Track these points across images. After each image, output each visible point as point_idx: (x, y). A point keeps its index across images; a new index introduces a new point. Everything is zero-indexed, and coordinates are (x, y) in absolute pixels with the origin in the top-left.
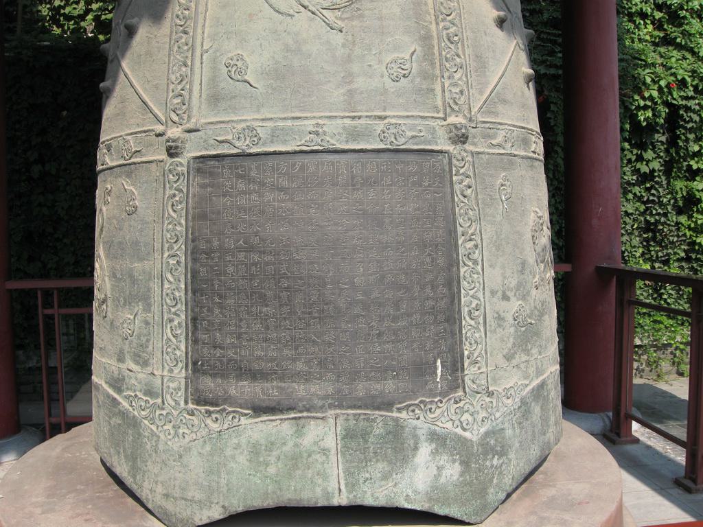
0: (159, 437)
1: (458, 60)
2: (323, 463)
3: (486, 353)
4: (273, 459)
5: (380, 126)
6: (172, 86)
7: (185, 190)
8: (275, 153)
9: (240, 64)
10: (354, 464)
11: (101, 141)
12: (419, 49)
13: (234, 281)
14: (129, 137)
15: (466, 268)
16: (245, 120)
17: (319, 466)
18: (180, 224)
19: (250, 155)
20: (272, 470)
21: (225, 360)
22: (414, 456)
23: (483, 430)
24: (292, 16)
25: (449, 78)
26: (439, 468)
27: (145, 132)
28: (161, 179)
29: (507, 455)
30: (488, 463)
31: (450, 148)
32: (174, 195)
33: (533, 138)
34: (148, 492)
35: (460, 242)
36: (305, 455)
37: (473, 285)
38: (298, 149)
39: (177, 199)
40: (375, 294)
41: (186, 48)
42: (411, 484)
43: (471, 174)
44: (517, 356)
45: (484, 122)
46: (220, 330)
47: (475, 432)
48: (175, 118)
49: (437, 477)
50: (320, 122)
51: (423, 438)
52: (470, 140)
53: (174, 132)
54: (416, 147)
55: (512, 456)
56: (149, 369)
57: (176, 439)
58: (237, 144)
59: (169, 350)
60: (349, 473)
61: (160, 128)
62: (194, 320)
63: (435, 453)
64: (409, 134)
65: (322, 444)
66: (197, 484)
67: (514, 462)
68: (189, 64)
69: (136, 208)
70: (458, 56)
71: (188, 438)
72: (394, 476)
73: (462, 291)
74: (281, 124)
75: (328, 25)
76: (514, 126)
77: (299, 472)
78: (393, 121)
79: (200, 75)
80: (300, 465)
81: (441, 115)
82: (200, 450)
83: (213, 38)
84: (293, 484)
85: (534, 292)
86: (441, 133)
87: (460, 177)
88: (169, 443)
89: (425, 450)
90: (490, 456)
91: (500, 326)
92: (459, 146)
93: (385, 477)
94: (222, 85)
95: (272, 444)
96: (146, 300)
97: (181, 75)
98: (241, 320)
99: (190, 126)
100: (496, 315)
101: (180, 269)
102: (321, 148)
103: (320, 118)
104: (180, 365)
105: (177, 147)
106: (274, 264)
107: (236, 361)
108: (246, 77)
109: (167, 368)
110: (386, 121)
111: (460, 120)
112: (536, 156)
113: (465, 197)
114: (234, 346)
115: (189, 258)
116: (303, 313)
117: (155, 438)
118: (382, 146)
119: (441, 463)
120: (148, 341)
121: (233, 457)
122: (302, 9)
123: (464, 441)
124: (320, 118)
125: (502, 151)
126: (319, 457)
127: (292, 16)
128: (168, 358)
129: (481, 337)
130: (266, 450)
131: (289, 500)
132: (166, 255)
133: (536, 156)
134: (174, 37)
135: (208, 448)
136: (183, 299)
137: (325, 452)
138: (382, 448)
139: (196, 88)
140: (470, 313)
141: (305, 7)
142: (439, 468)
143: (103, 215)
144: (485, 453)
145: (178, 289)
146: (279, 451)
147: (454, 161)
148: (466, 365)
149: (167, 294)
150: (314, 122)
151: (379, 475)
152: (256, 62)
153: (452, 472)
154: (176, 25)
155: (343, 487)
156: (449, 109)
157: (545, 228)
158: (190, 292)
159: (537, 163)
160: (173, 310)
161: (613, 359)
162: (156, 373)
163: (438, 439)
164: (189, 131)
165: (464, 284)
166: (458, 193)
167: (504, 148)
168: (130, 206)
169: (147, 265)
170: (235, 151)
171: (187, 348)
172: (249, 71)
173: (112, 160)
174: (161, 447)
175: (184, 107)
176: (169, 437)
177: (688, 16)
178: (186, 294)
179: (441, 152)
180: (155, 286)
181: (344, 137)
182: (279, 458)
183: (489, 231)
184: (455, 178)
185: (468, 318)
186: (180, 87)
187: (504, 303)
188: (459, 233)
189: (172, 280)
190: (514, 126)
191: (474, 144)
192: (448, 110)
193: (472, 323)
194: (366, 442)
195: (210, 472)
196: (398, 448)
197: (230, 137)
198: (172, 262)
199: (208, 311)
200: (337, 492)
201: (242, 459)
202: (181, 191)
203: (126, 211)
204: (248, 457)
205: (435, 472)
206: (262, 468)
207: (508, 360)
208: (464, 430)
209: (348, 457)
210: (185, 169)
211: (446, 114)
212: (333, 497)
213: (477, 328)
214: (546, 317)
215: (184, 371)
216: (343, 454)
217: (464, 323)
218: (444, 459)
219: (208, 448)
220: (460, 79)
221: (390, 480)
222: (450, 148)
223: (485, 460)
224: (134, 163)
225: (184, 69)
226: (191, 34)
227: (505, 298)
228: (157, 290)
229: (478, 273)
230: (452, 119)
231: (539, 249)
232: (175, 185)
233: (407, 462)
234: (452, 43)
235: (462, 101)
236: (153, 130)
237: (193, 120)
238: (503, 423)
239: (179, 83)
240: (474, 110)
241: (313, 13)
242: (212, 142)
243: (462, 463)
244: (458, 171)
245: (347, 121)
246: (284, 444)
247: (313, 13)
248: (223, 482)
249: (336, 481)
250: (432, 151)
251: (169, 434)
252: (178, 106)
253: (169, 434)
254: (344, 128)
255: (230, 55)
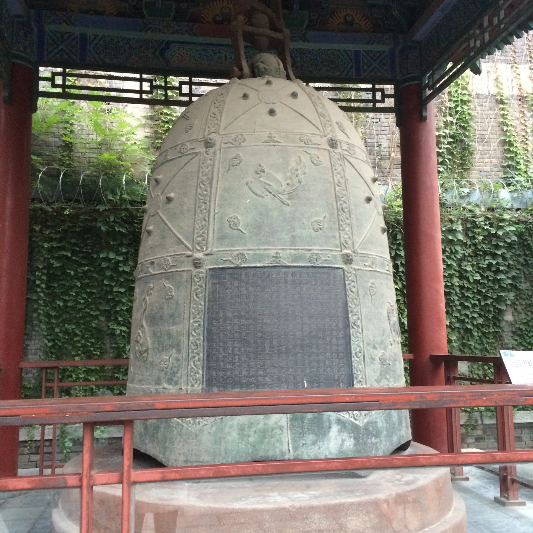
0: (183, 426)
1: (347, 221)
2: (280, 434)
3: (366, 377)
4: (252, 433)
5: (308, 254)
6: (196, 231)
7: (204, 286)
8: (255, 267)
9: (236, 221)
10: (297, 435)
11: (139, 263)
12: (327, 215)
13: (231, 334)
14: (168, 258)
15: (353, 330)
16: (238, 250)
17: (278, 436)
18: (201, 304)
19: (242, 268)
20: (251, 439)
21: (225, 377)
22: (329, 432)
23: (365, 421)
24: (263, 197)
25: (343, 230)
26: (343, 441)
27: (179, 255)
28: (190, 280)
29: (380, 438)
30: (369, 441)
31: (344, 266)
32: (198, 289)
33: (387, 263)
34: (174, 461)
35: (350, 316)
36: (270, 430)
37: (357, 339)
38: (267, 265)
39: (199, 290)
40: (307, 342)
41: (205, 211)
42: (328, 448)
43: (355, 280)
44: (382, 381)
45: (361, 253)
46: (223, 361)
47: (361, 422)
48: (199, 248)
49: (342, 445)
50: (279, 251)
51: (333, 422)
52: (353, 262)
53: (199, 255)
54: (327, 265)
55: (383, 438)
56: (178, 387)
57: (194, 426)
58: (235, 262)
59: (192, 374)
60: (294, 441)
61: (189, 253)
62: (208, 356)
63: (340, 431)
64: (323, 258)
65: (279, 424)
66: (206, 451)
67: (384, 442)
68: (207, 220)
69: (172, 296)
70: (347, 219)
71: (201, 424)
72: (319, 443)
73: (352, 342)
74: (258, 252)
75: (282, 202)
76: (377, 256)
77: (267, 440)
78: (315, 252)
79: (213, 226)
80: (267, 436)
81: (339, 249)
82: (209, 431)
83: (220, 206)
84: (263, 447)
85: (390, 346)
86: (340, 259)
87: (349, 282)
88: (190, 429)
89: (335, 428)
90: (370, 437)
91: (372, 363)
92: (349, 266)
93: (314, 443)
94: (226, 231)
95: (252, 424)
96: (178, 347)
97: (202, 226)
98: (235, 355)
99: (207, 252)
100: (370, 357)
101: (200, 329)
102: (278, 265)
103: (279, 249)
104: (199, 382)
105: (200, 263)
106: (254, 325)
107: (232, 377)
108: (239, 228)
109: (190, 384)
110: (311, 252)
111: (348, 252)
112: (388, 272)
113: (352, 292)
114: (231, 369)
115: (206, 323)
116: (269, 351)
117: (180, 427)
118: (310, 265)
119: (344, 437)
120: (178, 370)
121: (229, 433)
122: (268, 194)
123: (356, 427)
124: (279, 249)
125: (371, 269)
126: (278, 431)
127: (263, 197)
128: (191, 378)
129: (362, 368)
130: (248, 428)
131: (261, 457)
132: (192, 321)
133: (388, 272)
134: (197, 205)
135: (214, 429)
136: (202, 345)
137: (281, 428)
138: (311, 426)
139: (211, 232)
140: (356, 354)
141: (270, 193)
142: (343, 441)
143: (146, 302)
144: (368, 435)
145: (199, 340)
146: (255, 428)
147: (346, 273)
148: (355, 382)
149: (192, 343)
150: (275, 251)
151: (310, 442)
152: (243, 220)
153: (349, 444)
154: (199, 199)
155: (291, 449)
156: (343, 245)
157: (395, 312)
158: (206, 341)
159: (389, 277)
160: (195, 351)
161: (446, 422)
162: (183, 388)
163: (341, 423)
164: (207, 255)
165: (352, 338)
166: (349, 289)
167: (371, 267)
168: (168, 295)
169: (179, 328)
170: (233, 266)
171: (203, 372)
172: (241, 225)
173: (154, 271)
174: (184, 432)
175: (204, 242)
176: (190, 425)
177: (72, 163)
178: (204, 342)
179: (339, 268)
180: (184, 339)
181: (290, 260)
182: (255, 432)
183: (364, 311)
184: (347, 282)
185: (355, 357)
186: (201, 232)
187: (374, 351)
188: (349, 311)
189: (195, 334)
190: (377, 256)
191: (356, 265)
192: (343, 247)
193: (358, 359)
194: (303, 422)
195: (215, 443)
196: (321, 431)
197: (230, 258)
198: (196, 325)
199: (216, 351)
200: (287, 451)
201: (235, 434)
202: (201, 287)
203: (165, 298)
204: (238, 432)
205: (340, 442)
206: (245, 439)
207: (378, 383)
208: (355, 419)
209: (294, 431)
210: (204, 275)
211: (341, 249)
212: (286, 455)
213: (360, 363)
214: (397, 363)
215: (200, 385)
216: (291, 429)
217: (353, 359)
218: (345, 435)
219: (214, 429)
220: (349, 231)
221: (316, 445)
222: (344, 266)
223: (368, 438)
224: (171, 272)
225: (204, 222)
226: (208, 204)
227: (374, 347)
228: (186, 341)
229: (360, 333)
230: (345, 251)
231: (392, 323)
232: (198, 284)
233: (325, 435)
234: (344, 212)
235: (350, 242)
236: (184, 254)
237: (210, 249)
238: (376, 418)
239: (201, 229)
240: (356, 247)
241: (274, 196)
242: (220, 261)
243: (355, 438)
244: (348, 279)
245: (292, 251)
246: (259, 424)
247: (274, 196)
248: (223, 448)
249: (287, 445)
250: (336, 268)
251: (190, 423)
252: (200, 242)
253: (190, 423)
254: (290, 254)
255: (230, 216)
